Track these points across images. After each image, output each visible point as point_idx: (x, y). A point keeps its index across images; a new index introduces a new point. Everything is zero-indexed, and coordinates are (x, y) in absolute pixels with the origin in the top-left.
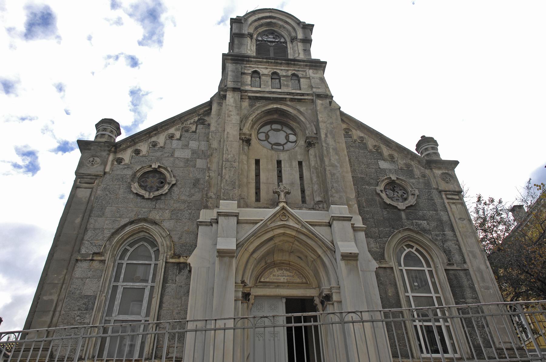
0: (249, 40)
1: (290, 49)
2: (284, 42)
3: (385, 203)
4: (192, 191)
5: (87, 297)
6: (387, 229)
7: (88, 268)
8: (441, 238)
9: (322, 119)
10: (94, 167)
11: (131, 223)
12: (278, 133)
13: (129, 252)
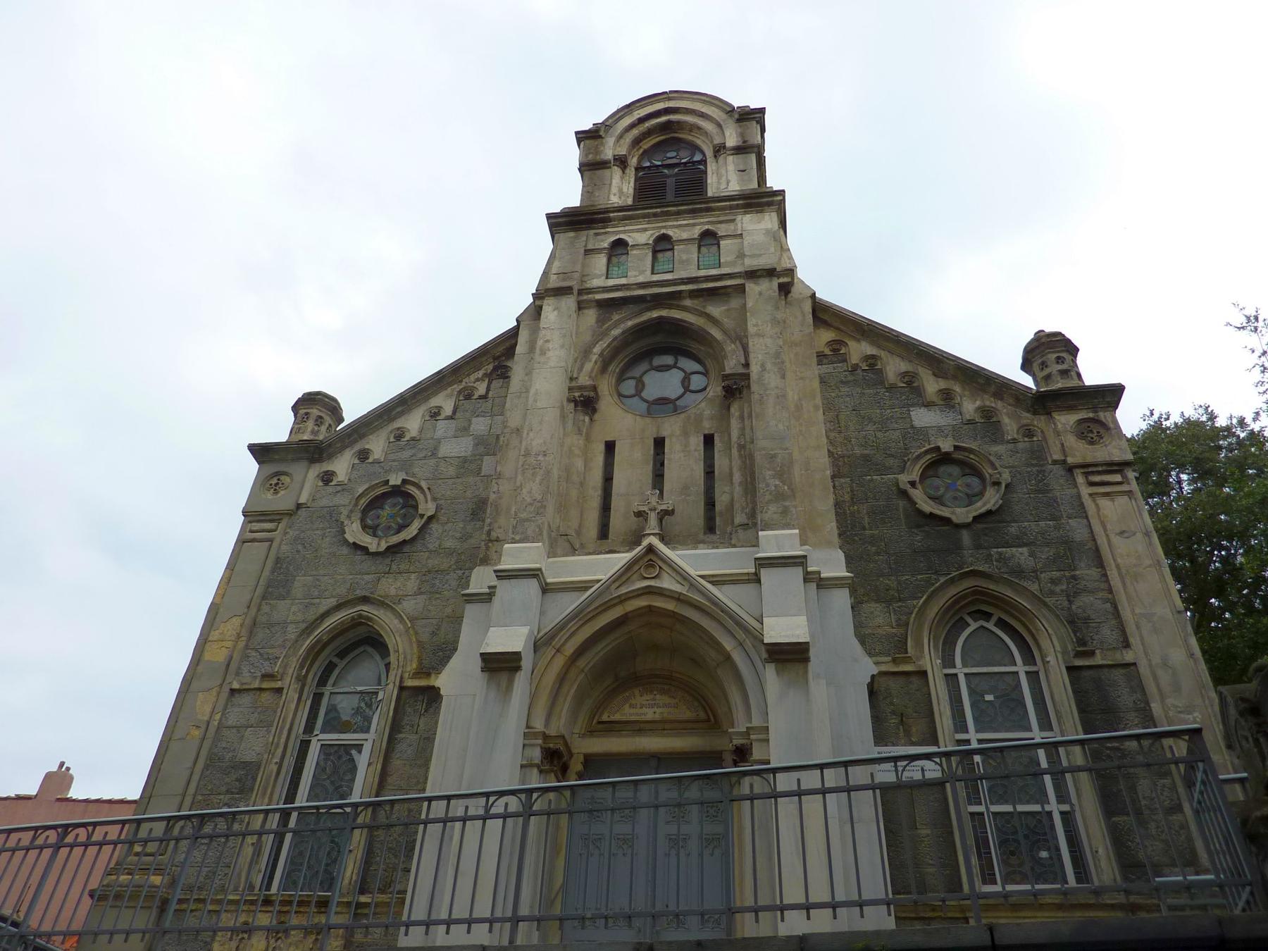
0: (616, 171)
1: (713, 173)
2: (699, 162)
3: (920, 513)
4: (468, 527)
5: (246, 764)
6: (919, 577)
7: (251, 705)
8: (1064, 587)
9: (756, 328)
10: (279, 495)
11: (338, 607)
12: (667, 374)
13: (337, 668)
